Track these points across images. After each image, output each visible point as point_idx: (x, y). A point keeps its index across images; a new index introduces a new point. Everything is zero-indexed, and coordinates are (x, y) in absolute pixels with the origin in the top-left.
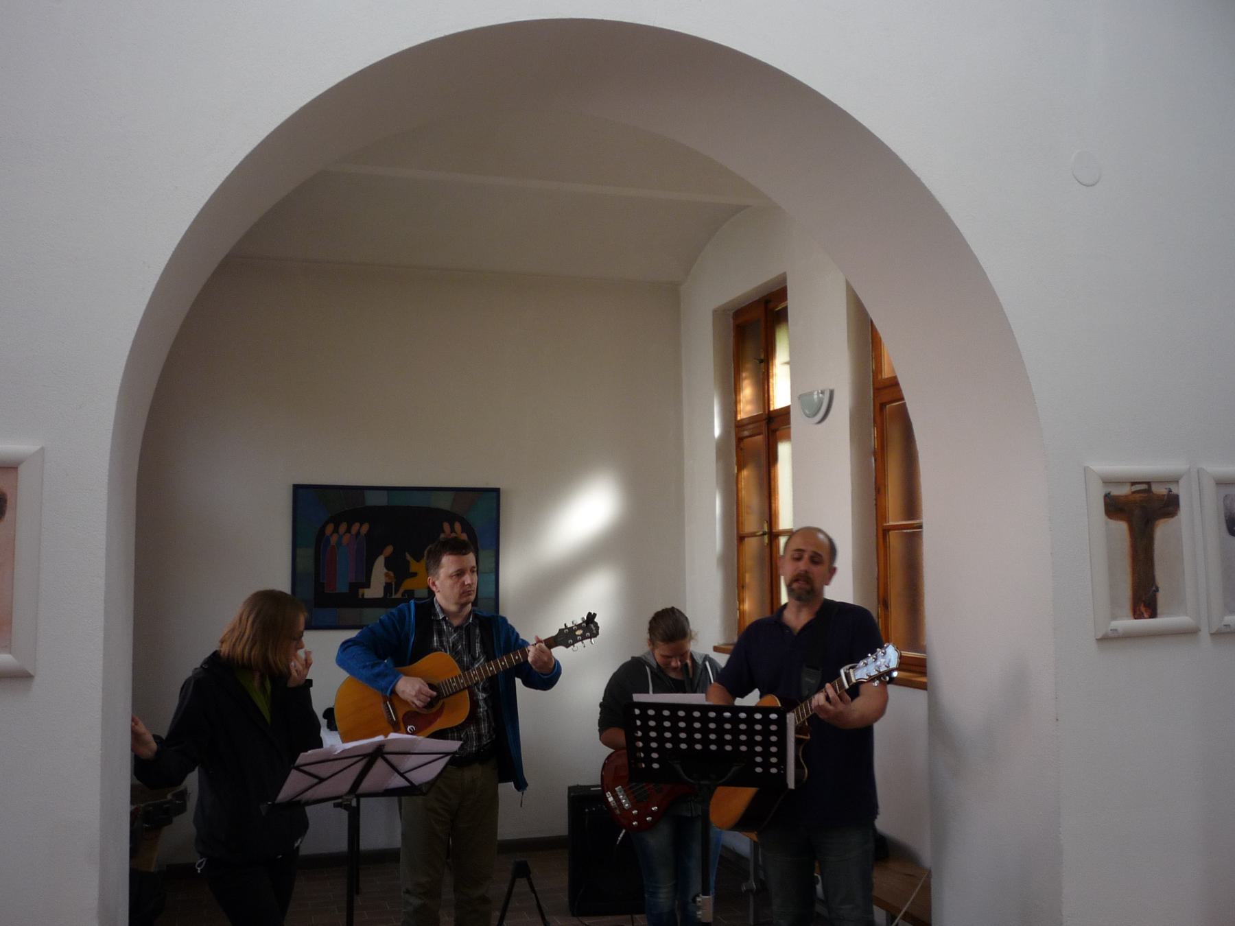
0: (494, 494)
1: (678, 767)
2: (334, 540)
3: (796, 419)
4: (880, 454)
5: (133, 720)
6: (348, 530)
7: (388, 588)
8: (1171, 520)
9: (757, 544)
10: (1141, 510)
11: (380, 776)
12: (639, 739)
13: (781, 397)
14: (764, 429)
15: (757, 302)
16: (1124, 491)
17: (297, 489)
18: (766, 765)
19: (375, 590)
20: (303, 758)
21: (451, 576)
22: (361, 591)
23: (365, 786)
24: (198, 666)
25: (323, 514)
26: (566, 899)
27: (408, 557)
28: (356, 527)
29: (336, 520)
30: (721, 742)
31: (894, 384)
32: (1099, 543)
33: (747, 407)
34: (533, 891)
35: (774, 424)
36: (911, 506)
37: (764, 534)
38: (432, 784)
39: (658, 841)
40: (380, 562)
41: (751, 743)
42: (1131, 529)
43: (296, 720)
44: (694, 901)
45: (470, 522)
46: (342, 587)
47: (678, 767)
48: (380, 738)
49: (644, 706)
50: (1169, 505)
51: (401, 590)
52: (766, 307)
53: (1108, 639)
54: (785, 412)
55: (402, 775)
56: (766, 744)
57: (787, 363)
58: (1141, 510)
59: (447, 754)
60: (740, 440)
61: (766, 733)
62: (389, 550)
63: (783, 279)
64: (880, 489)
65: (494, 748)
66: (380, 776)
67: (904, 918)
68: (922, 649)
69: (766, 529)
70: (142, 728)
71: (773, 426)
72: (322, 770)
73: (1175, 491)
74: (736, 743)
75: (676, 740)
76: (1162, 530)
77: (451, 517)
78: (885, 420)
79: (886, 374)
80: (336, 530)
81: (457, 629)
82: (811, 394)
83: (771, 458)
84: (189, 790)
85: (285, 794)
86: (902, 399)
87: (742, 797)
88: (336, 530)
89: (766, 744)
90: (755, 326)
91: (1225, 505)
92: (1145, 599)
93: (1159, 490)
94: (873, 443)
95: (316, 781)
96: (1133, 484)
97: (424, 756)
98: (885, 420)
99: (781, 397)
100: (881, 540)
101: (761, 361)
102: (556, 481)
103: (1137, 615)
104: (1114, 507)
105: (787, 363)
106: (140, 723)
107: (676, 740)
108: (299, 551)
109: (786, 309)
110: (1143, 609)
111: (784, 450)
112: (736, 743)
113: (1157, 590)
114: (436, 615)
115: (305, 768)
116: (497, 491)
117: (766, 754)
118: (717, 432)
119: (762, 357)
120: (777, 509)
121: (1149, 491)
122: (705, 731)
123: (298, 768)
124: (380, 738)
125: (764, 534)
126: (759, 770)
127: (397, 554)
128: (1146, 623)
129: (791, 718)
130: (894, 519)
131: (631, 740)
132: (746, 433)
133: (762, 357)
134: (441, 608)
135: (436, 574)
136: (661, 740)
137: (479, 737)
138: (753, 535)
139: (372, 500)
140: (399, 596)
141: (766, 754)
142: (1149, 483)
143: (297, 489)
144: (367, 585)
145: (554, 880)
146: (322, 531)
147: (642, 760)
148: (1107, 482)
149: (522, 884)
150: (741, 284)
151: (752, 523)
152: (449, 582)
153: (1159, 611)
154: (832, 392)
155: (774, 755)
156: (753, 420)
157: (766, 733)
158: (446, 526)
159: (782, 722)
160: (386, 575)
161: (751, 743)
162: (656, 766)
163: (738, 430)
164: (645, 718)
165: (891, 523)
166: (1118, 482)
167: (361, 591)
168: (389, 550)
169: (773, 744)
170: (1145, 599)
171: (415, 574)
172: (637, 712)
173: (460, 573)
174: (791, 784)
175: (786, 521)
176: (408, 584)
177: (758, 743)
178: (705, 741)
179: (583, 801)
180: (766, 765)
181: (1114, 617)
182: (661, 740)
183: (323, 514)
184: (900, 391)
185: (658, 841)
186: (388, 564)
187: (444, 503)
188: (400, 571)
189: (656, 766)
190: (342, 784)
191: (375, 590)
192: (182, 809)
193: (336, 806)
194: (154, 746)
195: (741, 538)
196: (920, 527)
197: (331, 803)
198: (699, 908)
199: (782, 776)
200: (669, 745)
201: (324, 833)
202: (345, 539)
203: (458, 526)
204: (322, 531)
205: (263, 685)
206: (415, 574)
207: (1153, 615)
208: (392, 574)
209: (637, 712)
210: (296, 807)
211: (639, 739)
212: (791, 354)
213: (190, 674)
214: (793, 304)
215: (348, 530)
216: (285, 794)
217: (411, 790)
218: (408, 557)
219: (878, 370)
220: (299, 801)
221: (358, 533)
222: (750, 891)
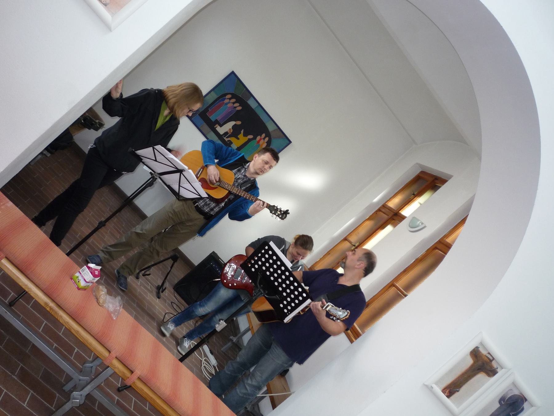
0: (288, 142)
1: (259, 277)
2: (226, 101)
3: (404, 223)
4: (418, 261)
5: (117, 85)
6: (234, 103)
7: (226, 133)
8: (487, 377)
9: (352, 245)
10: (482, 364)
11: (172, 180)
12: (254, 260)
13: (407, 212)
14: (390, 215)
15: (432, 176)
16: (484, 352)
17: (233, 73)
18: (285, 307)
19: (221, 130)
20: (159, 147)
21: (263, 161)
22: (217, 125)
23: (165, 177)
24: (155, 88)
25: (233, 89)
26: (176, 282)
27: (242, 132)
28: (238, 104)
29: (234, 96)
30: (280, 285)
31: (448, 247)
32: (457, 357)
33: (393, 204)
34: (171, 268)
35: (394, 217)
36: (410, 286)
37: (354, 246)
38: (186, 200)
39: (224, 294)
40: (233, 123)
41: (289, 295)
42: (472, 366)
43: (165, 134)
44: (220, 320)
45: (275, 143)
46: (213, 118)
47: (259, 277)
48: (186, 167)
49: (270, 248)
50: (492, 372)
51: (229, 139)
52: (433, 181)
53: (430, 389)
54: (403, 218)
55: (179, 186)
56: (293, 300)
57: (421, 204)
58: (482, 364)
59: (200, 195)
60: (379, 210)
61: (296, 297)
62: (239, 123)
63: (450, 177)
64: (406, 271)
65: (205, 217)
66: (172, 180)
67: (270, 397)
68: (363, 332)
69: (356, 245)
70: (120, 86)
71: (395, 218)
72: (159, 158)
73: (498, 370)
74: (284, 290)
75: (268, 269)
76: (481, 376)
77: (268, 134)
78: (438, 250)
79: (449, 240)
80: (230, 99)
81: (245, 176)
82: (418, 220)
83: (382, 227)
84: (104, 126)
85: (140, 152)
86: (446, 254)
87: (266, 306)
88: (230, 99)
89: (293, 300)
90: (426, 182)
91: (507, 392)
92: (451, 390)
93: (494, 364)
94: (419, 255)
95: (154, 159)
96: (489, 353)
97: (192, 188)
98: (438, 250)
99: (407, 212)
100: (387, 287)
101: (414, 194)
102: (313, 159)
103: (444, 391)
104: (475, 353)
105: (421, 204)
106: (121, 84)
107: (268, 269)
108: (212, 93)
109: (440, 187)
110: (447, 391)
111: (389, 228)
112: (284, 290)
113: (458, 391)
114: (245, 165)
115: (155, 150)
116: (290, 142)
117: (289, 304)
118: (376, 200)
119: (416, 193)
120: (367, 242)
121: (491, 361)
122: (280, 276)
123: (154, 148)
124: (186, 167)
125: (354, 246)
126: (281, 306)
127: (242, 126)
128: (443, 396)
129: (309, 301)
130: (399, 284)
131: (252, 257)
132: (383, 210)
133: (416, 193)
134: (248, 166)
135: (259, 155)
136: (264, 264)
137: (212, 209)
138: (350, 242)
139: (251, 102)
140: (227, 140)
141: (289, 304)
142: (494, 359)
143: (233, 73)
144: (221, 126)
145: (179, 273)
146: (225, 95)
147: (251, 264)
148: (481, 343)
149: (170, 262)
150: (435, 165)
151: (354, 239)
152: (260, 161)
153: (452, 397)
154: (425, 227)
155: (299, 300)
156: (390, 209)
157: (296, 297)
158: (264, 135)
159: (305, 299)
160: (230, 129)
161: (289, 295)
162: (253, 270)
163: (383, 208)
164: (267, 252)
165: (397, 285)
166: (485, 348)
167: (217, 125)
168: (239, 123)
169: (295, 303)
170: (451, 390)
171: (238, 139)
172: (267, 248)
173: (267, 163)
174: (287, 320)
175: (369, 246)
176: (233, 139)
177: (294, 295)
178: (276, 279)
179: (213, 258)
180: (285, 307)
181: (437, 383)
182: (264, 264)
183: (233, 89)
184: (448, 251)
185: (224, 294)
186: (234, 127)
187: (271, 128)
188: (235, 132)
189: (253, 270)
190: (160, 169)
191: (221, 130)
192: (97, 129)
193: (151, 173)
194: (118, 95)
195: (345, 239)
196: (406, 296)
197: (150, 171)
198: (219, 324)
199: (286, 315)
200: (264, 268)
201: (128, 183)
202: (230, 105)
203: (267, 139)
204: (225, 95)
205: (166, 116)
206: (238, 139)
207: (448, 397)
208: (232, 131)
209: (267, 248)
210: (139, 159)
211: (254, 260)
212: (425, 202)
213: (149, 88)
214: (443, 189)
215: (234, 103)
216: (140, 152)
217: (177, 194)
218: (242, 132)
219: (447, 236)
220: (142, 159)
221: (235, 107)
222: (232, 340)
